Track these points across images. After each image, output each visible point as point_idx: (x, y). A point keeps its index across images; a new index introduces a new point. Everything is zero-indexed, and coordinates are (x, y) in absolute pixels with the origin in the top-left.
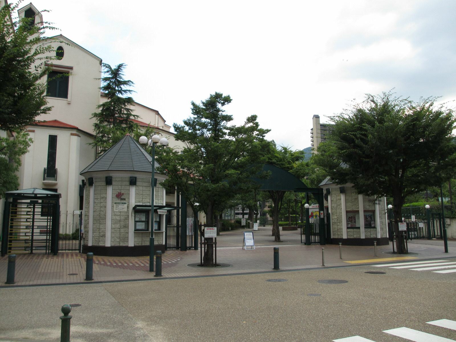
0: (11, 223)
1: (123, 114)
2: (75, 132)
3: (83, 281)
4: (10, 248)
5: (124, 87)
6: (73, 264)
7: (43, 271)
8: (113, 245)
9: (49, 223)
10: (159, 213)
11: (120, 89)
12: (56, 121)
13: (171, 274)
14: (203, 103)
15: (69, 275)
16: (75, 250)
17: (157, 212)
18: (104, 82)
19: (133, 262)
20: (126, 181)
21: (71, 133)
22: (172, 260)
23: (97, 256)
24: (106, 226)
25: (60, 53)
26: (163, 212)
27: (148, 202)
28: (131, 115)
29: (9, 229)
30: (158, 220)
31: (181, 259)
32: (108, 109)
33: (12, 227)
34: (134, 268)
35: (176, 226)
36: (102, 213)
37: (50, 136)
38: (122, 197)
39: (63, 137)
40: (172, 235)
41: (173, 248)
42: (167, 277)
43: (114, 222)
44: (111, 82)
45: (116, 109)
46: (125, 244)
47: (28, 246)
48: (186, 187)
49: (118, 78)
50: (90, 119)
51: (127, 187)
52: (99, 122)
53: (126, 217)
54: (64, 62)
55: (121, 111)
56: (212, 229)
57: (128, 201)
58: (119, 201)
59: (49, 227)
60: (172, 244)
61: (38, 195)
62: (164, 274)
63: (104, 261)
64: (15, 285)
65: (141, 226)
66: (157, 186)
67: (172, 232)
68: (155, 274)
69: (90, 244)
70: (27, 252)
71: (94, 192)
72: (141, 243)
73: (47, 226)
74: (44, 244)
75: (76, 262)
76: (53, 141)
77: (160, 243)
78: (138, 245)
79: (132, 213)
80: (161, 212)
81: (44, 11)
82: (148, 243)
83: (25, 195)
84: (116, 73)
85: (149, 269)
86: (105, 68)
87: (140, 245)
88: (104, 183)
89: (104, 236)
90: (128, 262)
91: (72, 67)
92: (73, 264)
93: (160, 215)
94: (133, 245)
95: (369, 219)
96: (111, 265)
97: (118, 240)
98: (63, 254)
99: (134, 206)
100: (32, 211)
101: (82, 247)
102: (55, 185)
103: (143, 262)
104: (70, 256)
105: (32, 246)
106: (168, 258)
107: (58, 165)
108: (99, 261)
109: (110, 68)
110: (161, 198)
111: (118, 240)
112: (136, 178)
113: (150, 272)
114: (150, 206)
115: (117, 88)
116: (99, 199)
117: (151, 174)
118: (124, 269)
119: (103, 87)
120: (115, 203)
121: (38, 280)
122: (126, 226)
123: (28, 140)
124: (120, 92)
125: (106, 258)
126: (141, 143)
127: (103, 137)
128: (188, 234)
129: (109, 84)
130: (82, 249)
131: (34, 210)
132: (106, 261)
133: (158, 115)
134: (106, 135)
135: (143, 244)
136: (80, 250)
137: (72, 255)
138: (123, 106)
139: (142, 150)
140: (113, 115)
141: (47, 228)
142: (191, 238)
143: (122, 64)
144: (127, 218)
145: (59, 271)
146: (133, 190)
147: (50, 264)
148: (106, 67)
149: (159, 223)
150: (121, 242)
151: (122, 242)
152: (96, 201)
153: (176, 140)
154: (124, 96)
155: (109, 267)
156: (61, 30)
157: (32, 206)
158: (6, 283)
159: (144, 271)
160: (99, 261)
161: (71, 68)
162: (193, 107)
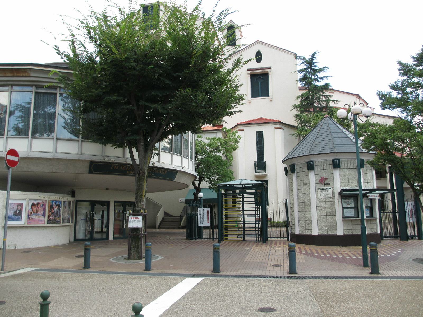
0: (225, 213)
1: (323, 101)
2: (278, 125)
3: (286, 274)
4: (226, 236)
5: (320, 75)
6: (279, 254)
7: (249, 260)
8: (320, 233)
9: (256, 211)
10: (370, 198)
11: (316, 77)
12: (261, 119)
13: (391, 272)
14: (414, 58)
15: (272, 265)
16: (284, 238)
17: (367, 197)
18: (300, 74)
19: (343, 253)
20: (328, 165)
21: (275, 127)
22: (390, 252)
23: (304, 245)
24: (311, 213)
26: (374, 196)
27: (356, 186)
28: (330, 100)
29: (224, 218)
30: (369, 205)
31: (403, 251)
32: (307, 98)
33: (226, 216)
34: (344, 260)
35: (391, 211)
36: (306, 200)
37: (257, 132)
38: (326, 182)
39: (268, 131)
40: (388, 221)
41: (390, 237)
42: (387, 275)
43: (320, 209)
44: (307, 72)
45: (315, 97)
46: (333, 232)
47: (240, 233)
48: (401, 164)
49: (313, 68)
50: (291, 111)
51: (330, 171)
52: (299, 112)
53: (332, 203)
54: (263, 64)
55: (319, 98)
56: (137, 218)
57: (333, 186)
58: (323, 187)
59: (257, 216)
60: (389, 231)
61: (246, 186)
62: (383, 271)
63: (311, 251)
65: (350, 213)
66: (364, 168)
67: (387, 218)
68: (370, 271)
69: (297, 232)
70: (240, 239)
71: (297, 179)
72: (351, 231)
73: (255, 214)
74: (254, 232)
75: (282, 251)
76: (260, 135)
77: (374, 232)
78: (348, 234)
79: (338, 199)
80: (372, 196)
81: (233, 12)
82: (359, 232)
83: (235, 186)
84: (310, 63)
85: (362, 263)
86: (300, 60)
88: (306, 169)
89: (310, 224)
90: (337, 253)
91: (271, 67)
92: (276, 253)
93: (371, 200)
94: (342, 234)
95: (56, 209)
96: (319, 257)
98: (272, 242)
99: (339, 191)
100: (242, 201)
101: (289, 235)
102: (265, 176)
103: (355, 253)
104: (278, 245)
105: (244, 234)
106: (386, 249)
107: (267, 158)
108: (305, 250)
109: (305, 59)
110: (369, 180)
112: (339, 160)
113: (363, 268)
114: (357, 190)
115: (313, 77)
116: (302, 186)
117: (355, 154)
118: (332, 261)
119: (300, 79)
120: (319, 189)
121: (242, 270)
122: (333, 213)
123: (237, 137)
124: (316, 80)
125: (313, 248)
126: (339, 117)
127: (304, 126)
128: (407, 221)
129: (305, 75)
130: (289, 237)
131: (243, 200)
132: (314, 251)
133: (359, 98)
134: (307, 124)
135: (354, 233)
136: (288, 238)
137: (280, 244)
138: (321, 94)
139: (343, 130)
140: (312, 104)
141: (255, 217)
142: (412, 226)
143: (316, 52)
144: (333, 205)
145: (264, 260)
146: (337, 173)
147: (257, 252)
148: (301, 59)
149: (371, 209)
150: (328, 231)
151: (330, 230)
152: (299, 188)
153: (382, 109)
154: (320, 83)
155: (316, 259)
156: (238, 11)
157: (241, 196)
158: (213, 272)
159: (355, 265)
160: (305, 250)
161: (270, 68)
162: (400, 67)
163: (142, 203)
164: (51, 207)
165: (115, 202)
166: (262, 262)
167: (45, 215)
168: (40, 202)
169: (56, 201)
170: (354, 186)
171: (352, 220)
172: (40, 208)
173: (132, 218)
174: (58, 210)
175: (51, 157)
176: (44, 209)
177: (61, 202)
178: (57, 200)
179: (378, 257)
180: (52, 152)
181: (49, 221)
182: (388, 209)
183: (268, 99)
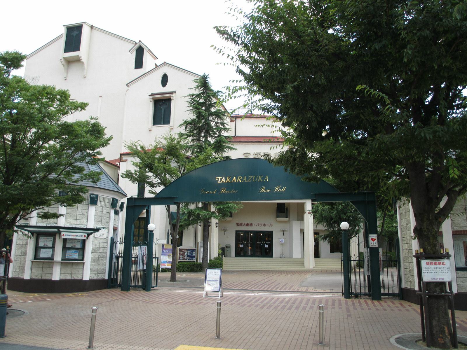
25: (165, 80)
72: (40, 275)
78: (36, 278)
87: (39, 277)
97: (18, 270)
111: (18, 270)
112: (97, 196)
135: (44, 278)
161: (172, 93)
170: (53, 222)
171: (43, 262)
179: (457, 325)
182: (136, 253)
183: (169, 127)
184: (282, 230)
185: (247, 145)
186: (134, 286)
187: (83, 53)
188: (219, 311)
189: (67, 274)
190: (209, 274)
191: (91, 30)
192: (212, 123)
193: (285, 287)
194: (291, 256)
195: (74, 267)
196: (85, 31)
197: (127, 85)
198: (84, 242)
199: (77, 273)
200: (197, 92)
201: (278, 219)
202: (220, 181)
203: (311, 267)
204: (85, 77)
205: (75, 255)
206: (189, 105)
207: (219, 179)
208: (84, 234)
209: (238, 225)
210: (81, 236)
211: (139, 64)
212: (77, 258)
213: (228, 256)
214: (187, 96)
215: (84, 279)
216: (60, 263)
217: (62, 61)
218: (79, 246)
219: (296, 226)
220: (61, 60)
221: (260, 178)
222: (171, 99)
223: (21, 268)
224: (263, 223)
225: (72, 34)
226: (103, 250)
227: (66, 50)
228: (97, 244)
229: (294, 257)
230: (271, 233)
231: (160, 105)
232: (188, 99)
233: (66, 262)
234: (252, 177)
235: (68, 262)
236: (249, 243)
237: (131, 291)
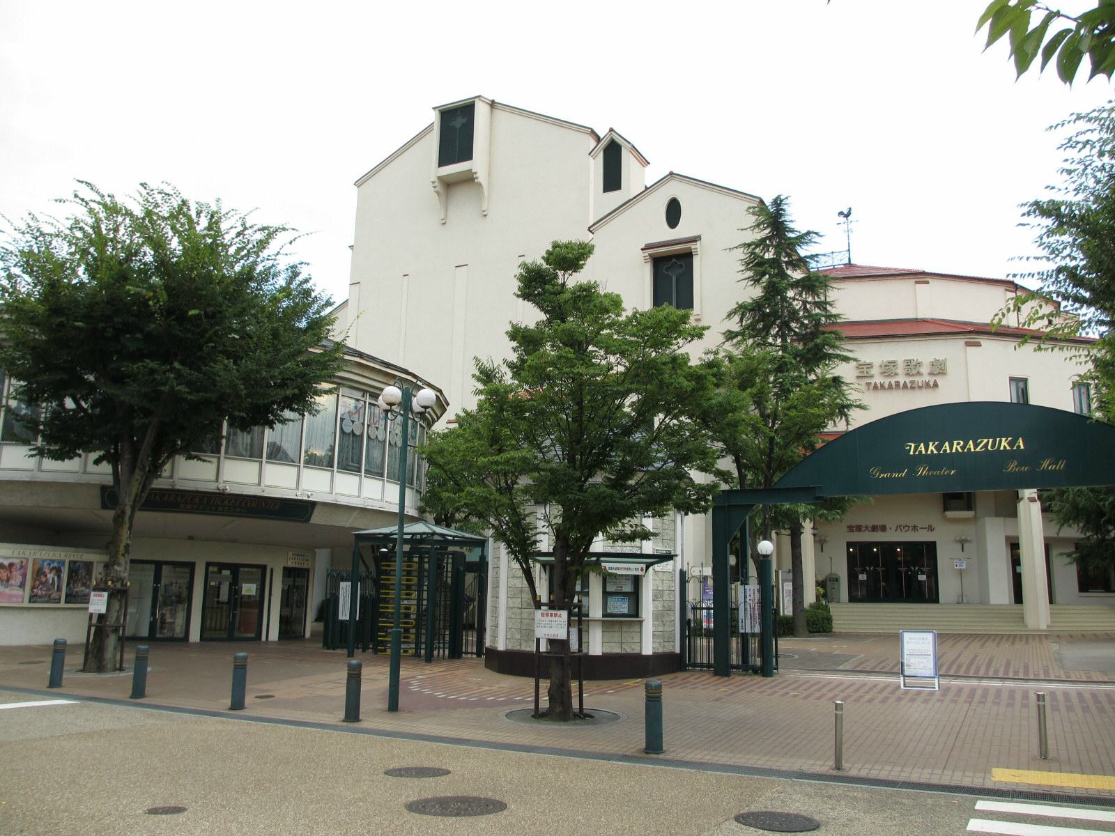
25: (673, 212)
54: (682, 231)
56: (556, 615)
64: (661, 756)
69: (501, 647)
94: (600, 654)
95: (50, 576)
97: (518, 636)
111: (518, 636)
161: (695, 240)
163: (116, 567)
164: (39, 573)
165: (208, 564)
166: (895, 764)
167: (24, 585)
168: (16, 561)
169: (53, 561)
172: (14, 573)
173: (543, 615)
174: (56, 578)
175: (28, 479)
176: (24, 576)
177: (63, 563)
178: (54, 558)
180: (33, 470)
181: (33, 598)
184: (958, 539)
185: (863, 345)
186: (695, 665)
187: (478, 164)
188: (838, 719)
189: (613, 644)
190: (908, 642)
191: (492, 111)
192: (795, 303)
193: (883, 664)
194: (984, 600)
195: (624, 629)
196: (481, 112)
197: (589, 228)
198: (637, 581)
199: (630, 640)
200: (758, 235)
201: (950, 514)
202: (914, 452)
203: (1043, 626)
204: (485, 216)
205: (623, 606)
206: (743, 268)
207: (911, 446)
208: (640, 566)
209: (851, 529)
210: (633, 568)
211: (612, 180)
212: (626, 611)
213: (835, 600)
214: (737, 247)
215: (644, 653)
216: (601, 623)
217: (436, 184)
218: (628, 588)
219: (994, 533)
220: (433, 183)
221: (1004, 443)
222: (691, 253)
223: (523, 632)
224: (911, 524)
225: (453, 123)
226: (669, 595)
227: (443, 162)
228: (659, 583)
229: (992, 602)
230: (931, 547)
231: (667, 269)
232: (741, 254)
233: (611, 621)
234: (985, 441)
235: (622, 621)
236: (880, 569)
237: (733, 676)
